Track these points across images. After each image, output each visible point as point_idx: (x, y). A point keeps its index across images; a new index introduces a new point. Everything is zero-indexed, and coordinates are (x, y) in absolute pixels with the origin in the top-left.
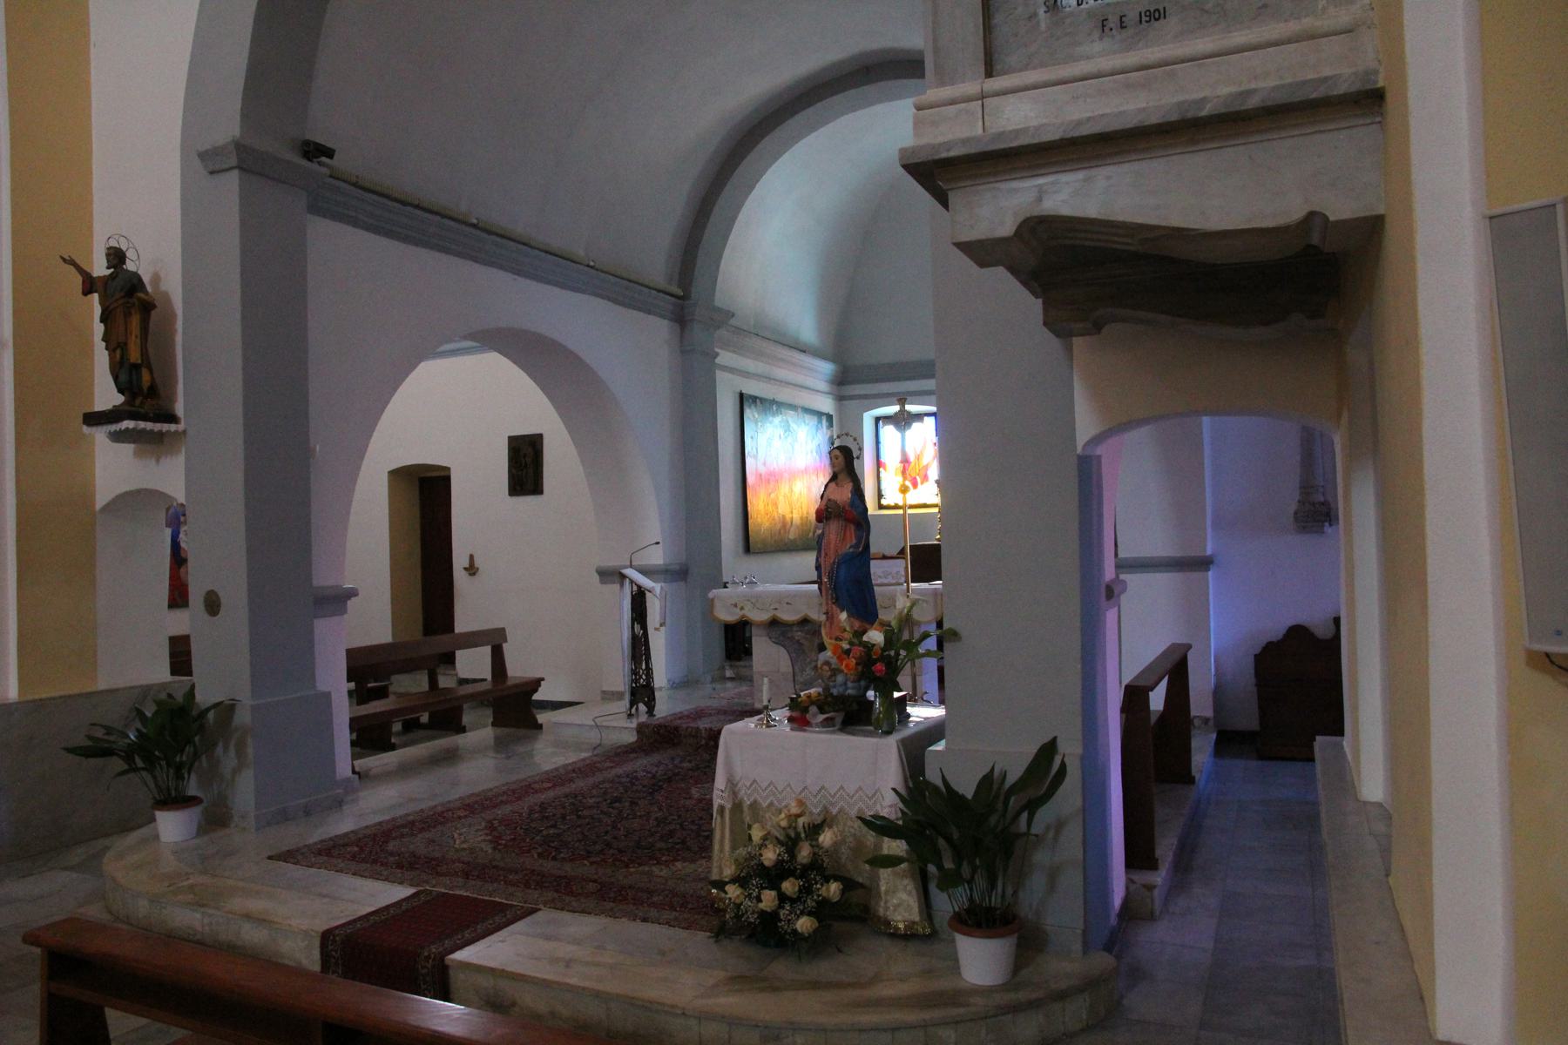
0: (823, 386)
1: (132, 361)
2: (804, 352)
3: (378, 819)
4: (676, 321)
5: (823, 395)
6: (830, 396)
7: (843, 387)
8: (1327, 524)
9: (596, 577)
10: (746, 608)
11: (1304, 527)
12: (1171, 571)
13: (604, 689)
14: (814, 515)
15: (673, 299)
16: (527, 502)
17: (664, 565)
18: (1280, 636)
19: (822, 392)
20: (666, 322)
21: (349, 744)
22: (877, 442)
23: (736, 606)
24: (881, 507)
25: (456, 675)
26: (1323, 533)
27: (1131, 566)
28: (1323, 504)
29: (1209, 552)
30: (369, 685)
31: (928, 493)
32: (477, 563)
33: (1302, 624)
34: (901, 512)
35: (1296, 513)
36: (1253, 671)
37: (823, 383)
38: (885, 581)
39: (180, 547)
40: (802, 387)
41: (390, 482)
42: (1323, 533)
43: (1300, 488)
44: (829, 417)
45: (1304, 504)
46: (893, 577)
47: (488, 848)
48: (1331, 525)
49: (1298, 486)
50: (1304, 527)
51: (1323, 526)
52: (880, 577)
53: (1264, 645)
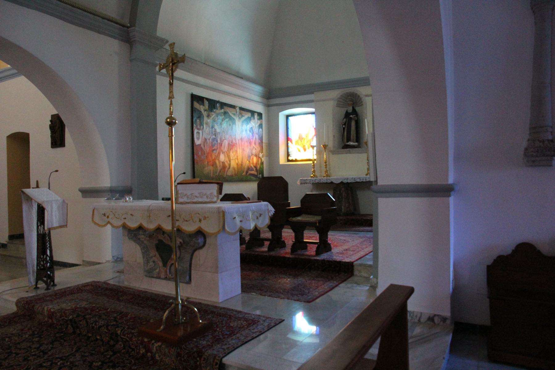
0: (258, 99)
2: (242, 78)
6: (262, 104)
7: (269, 100)
10: (110, 217)
11: (534, 161)
12: (424, 197)
13: (85, 259)
15: (118, 26)
16: (59, 150)
17: (110, 187)
18: (509, 251)
22: (287, 128)
23: (104, 215)
24: (289, 161)
29: (451, 181)
30: (334, 200)
31: (311, 154)
33: (527, 241)
34: (311, 162)
35: (526, 149)
36: (485, 280)
37: (257, 97)
38: (200, 200)
40: (244, 98)
42: (551, 166)
43: (530, 129)
44: (260, 115)
46: (207, 197)
50: (534, 161)
52: (196, 197)
53: (495, 258)
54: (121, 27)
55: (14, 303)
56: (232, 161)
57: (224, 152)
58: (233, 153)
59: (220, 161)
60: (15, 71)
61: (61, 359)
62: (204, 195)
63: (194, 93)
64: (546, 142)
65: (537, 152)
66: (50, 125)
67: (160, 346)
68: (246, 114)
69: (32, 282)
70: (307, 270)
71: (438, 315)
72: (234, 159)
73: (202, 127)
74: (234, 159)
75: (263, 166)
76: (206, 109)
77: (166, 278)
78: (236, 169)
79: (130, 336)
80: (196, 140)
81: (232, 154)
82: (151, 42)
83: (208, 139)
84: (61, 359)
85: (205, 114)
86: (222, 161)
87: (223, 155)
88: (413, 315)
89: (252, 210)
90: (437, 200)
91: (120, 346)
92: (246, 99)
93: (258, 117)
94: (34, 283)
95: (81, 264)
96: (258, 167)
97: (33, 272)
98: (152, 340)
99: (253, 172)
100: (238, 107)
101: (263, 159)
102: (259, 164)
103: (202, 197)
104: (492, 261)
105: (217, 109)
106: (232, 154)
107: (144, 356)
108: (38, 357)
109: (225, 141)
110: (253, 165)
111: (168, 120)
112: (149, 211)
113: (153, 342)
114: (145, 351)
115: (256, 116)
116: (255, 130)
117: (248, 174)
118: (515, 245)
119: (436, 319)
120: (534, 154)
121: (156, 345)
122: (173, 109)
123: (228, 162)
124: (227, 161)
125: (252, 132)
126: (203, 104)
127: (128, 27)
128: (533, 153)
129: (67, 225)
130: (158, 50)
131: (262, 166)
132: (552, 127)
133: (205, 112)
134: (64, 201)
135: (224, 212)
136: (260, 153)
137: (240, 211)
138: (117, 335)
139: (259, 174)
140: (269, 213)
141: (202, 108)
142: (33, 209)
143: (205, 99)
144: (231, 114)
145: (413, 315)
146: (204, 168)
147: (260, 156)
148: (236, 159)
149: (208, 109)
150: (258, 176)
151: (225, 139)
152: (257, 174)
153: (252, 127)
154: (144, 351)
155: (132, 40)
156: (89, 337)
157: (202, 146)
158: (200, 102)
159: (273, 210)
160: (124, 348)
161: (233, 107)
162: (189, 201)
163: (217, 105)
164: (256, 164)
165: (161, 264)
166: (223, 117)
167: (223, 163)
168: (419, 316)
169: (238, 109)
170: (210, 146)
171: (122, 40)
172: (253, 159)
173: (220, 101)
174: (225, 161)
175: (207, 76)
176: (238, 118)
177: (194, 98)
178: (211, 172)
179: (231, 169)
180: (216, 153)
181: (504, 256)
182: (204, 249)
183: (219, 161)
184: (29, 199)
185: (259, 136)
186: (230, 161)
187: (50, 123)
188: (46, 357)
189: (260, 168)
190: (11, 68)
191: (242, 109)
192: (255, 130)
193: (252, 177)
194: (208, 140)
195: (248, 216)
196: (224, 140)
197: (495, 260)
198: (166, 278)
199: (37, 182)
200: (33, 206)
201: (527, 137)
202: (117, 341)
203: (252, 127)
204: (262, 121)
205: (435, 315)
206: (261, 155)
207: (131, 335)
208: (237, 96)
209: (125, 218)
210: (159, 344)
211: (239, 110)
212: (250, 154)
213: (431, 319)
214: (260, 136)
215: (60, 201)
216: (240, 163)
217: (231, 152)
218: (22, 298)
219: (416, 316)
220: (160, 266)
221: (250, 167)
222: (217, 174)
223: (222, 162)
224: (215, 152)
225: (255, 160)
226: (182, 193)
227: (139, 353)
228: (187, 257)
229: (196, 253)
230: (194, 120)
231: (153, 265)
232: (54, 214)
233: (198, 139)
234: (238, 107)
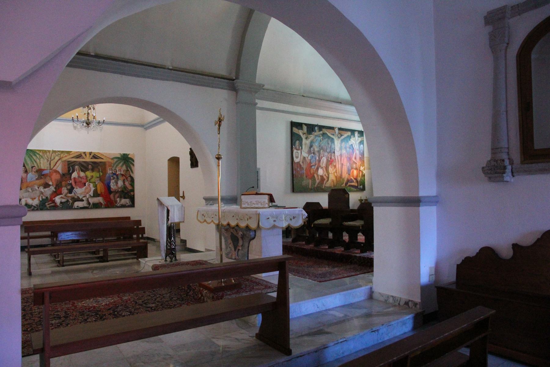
2: (341, 103)
4: (233, 90)
5: (359, 122)
9: (157, 199)
18: (474, 254)
19: (357, 121)
20: (225, 91)
21: (20, 248)
25: (180, 237)
27: (381, 202)
32: (185, 195)
33: (489, 246)
38: (256, 206)
39: (111, 187)
41: (169, 166)
46: (261, 204)
52: (254, 204)
54: (228, 81)
55: (151, 267)
56: (330, 175)
57: (323, 168)
58: (332, 168)
59: (318, 175)
60: (162, 119)
61: (160, 294)
62: (259, 203)
63: (294, 121)
64: (499, 162)
65: (491, 170)
66: (190, 152)
67: (206, 293)
68: (345, 134)
69: (163, 256)
70: (349, 264)
71: (412, 301)
72: (332, 173)
73: (301, 148)
74: (332, 173)
75: (364, 178)
76: (304, 132)
77: (235, 259)
78: (335, 182)
79: (195, 287)
80: (295, 159)
81: (331, 169)
82: (251, 88)
83: (307, 157)
84: (160, 294)
85: (303, 137)
86: (321, 175)
87: (322, 170)
88: (395, 299)
89: (285, 213)
90: (411, 209)
91: (191, 293)
92: (345, 120)
93: (359, 135)
94: (164, 258)
95: (204, 251)
96: (359, 179)
97: (164, 250)
98: (204, 289)
99: (353, 184)
100: (337, 128)
101: (364, 172)
102: (359, 176)
103: (257, 204)
104: (461, 261)
105: (316, 132)
106: (331, 169)
107: (200, 298)
108: (151, 292)
109: (323, 158)
110: (353, 178)
111: (217, 156)
112: (235, 215)
113: (204, 290)
115: (356, 134)
116: (356, 147)
117: (347, 185)
118: (479, 249)
119: (410, 303)
120: (489, 172)
121: (205, 292)
123: (327, 175)
124: (325, 175)
125: (352, 148)
126: (302, 129)
127: (234, 80)
128: (488, 171)
129: (184, 221)
130: (257, 93)
131: (364, 178)
133: (304, 135)
134: (182, 206)
135: (259, 214)
136: (361, 167)
137: (274, 214)
138: (190, 286)
139: (360, 185)
140: (303, 217)
141: (300, 132)
142: (164, 210)
143: (303, 125)
144: (329, 134)
145: (395, 299)
146: (302, 181)
147: (361, 169)
148: (334, 173)
149: (306, 132)
150: (359, 187)
151: (324, 156)
152: (358, 185)
153: (352, 144)
154: (200, 296)
155: (237, 88)
156: (179, 287)
157: (301, 163)
158: (299, 127)
159: (306, 214)
160: (193, 294)
161: (332, 128)
162: (249, 206)
163: (315, 128)
164: (357, 176)
165: (233, 249)
166: (322, 138)
167: (322, 176)
168: (399, 300)
169: (337, 130)
170: (309, 162)
171: (229, 90)
172: (353, 172)
173: (319, 124)
174: (323, 175)
175: (305, 105)
176: (337, 138)
177: (294, 125)
178: (309, 185)
179: (330, 181)
180: (314, 168)
181: (470, 257)
182: (255, 240)
183: (318, 175)
184: (82, 199)
185: (360, 152)
186: (328, 175)
187: (190, 150)
188: (154, 293)
189: (361, 179)
190: (159, 117)
191: (340, 129)
192: (356, 147)
193: (352, 188)
194: (306, 158)
195: (282, 218)
196: (322, 157)
197: (463, 260)
198: (235, 259)
199: (183, 192)
200: (164, 208)
202: (190, 290)
203: (352, 144)
204: (363, 138)
205: (409, 301)
206: (362, 168)
207: (196, 286)
208: (337, 118)
209: (213, 218)
210: (206, 291)
211: (337, 130)
212: (350, 168)
213: (407, 303)
214: (362, 151)
215: (180, 205)
216: (339, 175)
217: (330, 167)
218: (155, 264)
219: (397, 300)
220: (255, 256)
221: (349, 179)
222: (316, 186)
223: (321, 176)
224: (313, 167)
225: (355, 172)
226: (244, 201)
227: (198, 297)
228: (247, 245)
229: (251, 242)
230: (293, 143)
231: (230, 250)
232: (175, 213)
233: (297, 157)
234: (337, 128)
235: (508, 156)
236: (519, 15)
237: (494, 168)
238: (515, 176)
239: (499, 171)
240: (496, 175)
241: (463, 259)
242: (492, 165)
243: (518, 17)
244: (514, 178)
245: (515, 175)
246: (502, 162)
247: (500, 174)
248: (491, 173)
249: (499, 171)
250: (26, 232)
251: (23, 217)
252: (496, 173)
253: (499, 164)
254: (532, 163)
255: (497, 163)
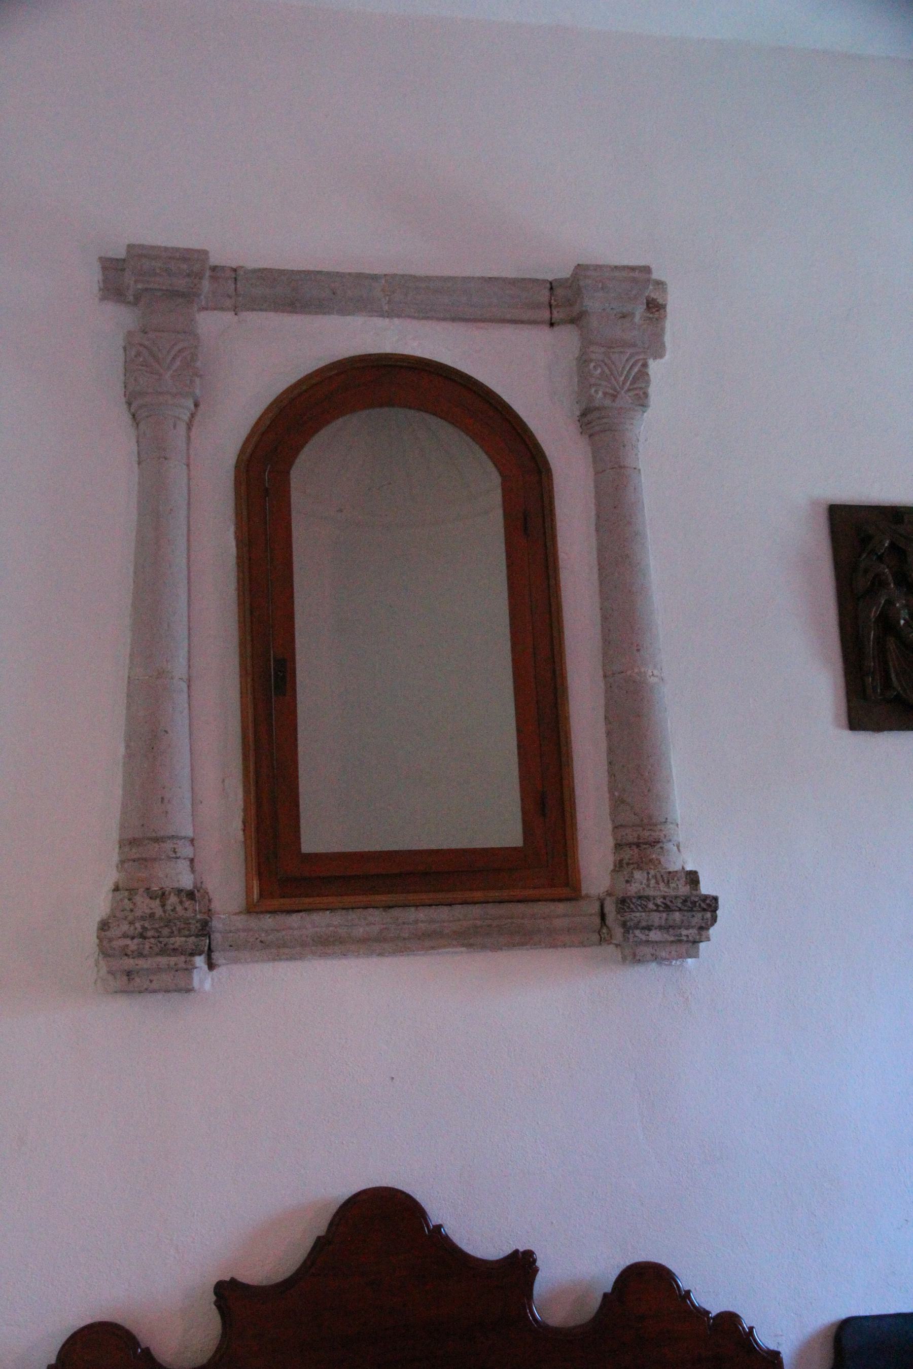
1: (210, 264)
3: (465, 436)
8: (200, 961)
14: (600, 1299)
26: (189, 990)
28: (191, 895)
30: (427, 1233)
33: (106, 1318)
35: (104, 926)
42: (189, 990)
45: (132, 891)
47: (204, 955)
48: (211, 966)
49: (115, 836)
51: (189, 969)
64: (173, 899)
114: (896, 604)
120: (133, 945)
122: (763, 1344)
128: (128, 942)
132: (192, 841)
181: (225, 1282)
201: (112, 876)
235: (192, 876)
236: (236, 310)
237: (156, 930)
238: (219, 966)
239: (178, 941)
240: (163, 960)
241: (214, 1298)
242: (138, 913)
243: (229, 316)
244: (215, 972)
245: (221, 961)
246: (187, 904)
247: (183, 958)
248: (141, 955)
249: (178, 941)
250: (705, 898)
251: (701, 943)
252: (164, 951)
253: (174, 910)
254: (290, 912)
255: (163, 906)
